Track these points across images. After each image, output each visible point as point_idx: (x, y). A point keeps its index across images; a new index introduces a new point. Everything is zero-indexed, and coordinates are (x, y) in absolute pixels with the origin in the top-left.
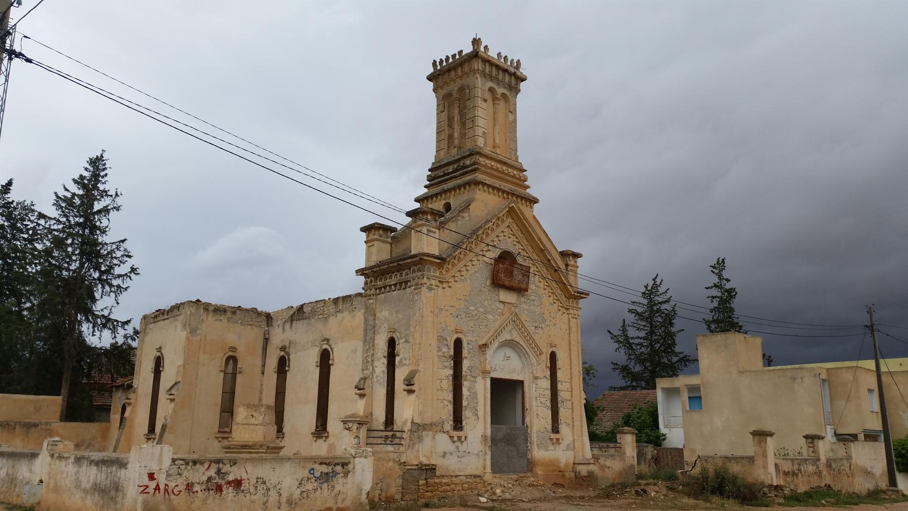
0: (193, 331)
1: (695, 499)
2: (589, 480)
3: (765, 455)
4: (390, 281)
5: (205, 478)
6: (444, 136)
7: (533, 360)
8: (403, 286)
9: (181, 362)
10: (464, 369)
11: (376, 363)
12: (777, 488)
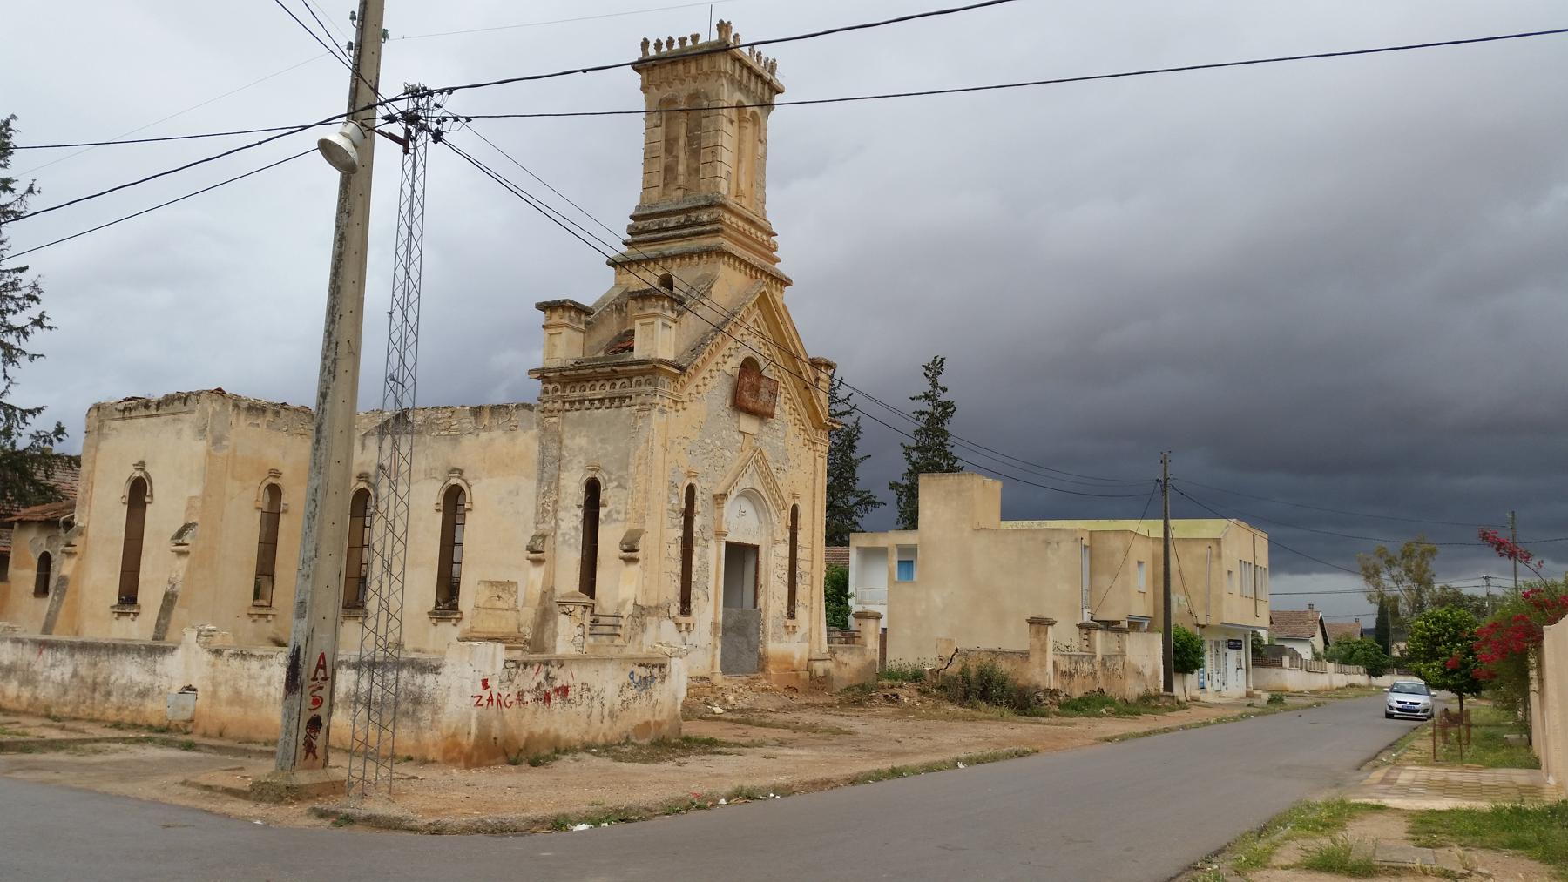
0: (217, 441)
1: (961, 705)
2: (819, 683)
3: (1044, 651)
4: (598, 392)
5: (534, 685)
6: (659, 165)
7: (774, 518)
8: (617, 403)
9: (197, 491)
10: (696, 529)
11: (561, 514)
12: (1053, 693)
